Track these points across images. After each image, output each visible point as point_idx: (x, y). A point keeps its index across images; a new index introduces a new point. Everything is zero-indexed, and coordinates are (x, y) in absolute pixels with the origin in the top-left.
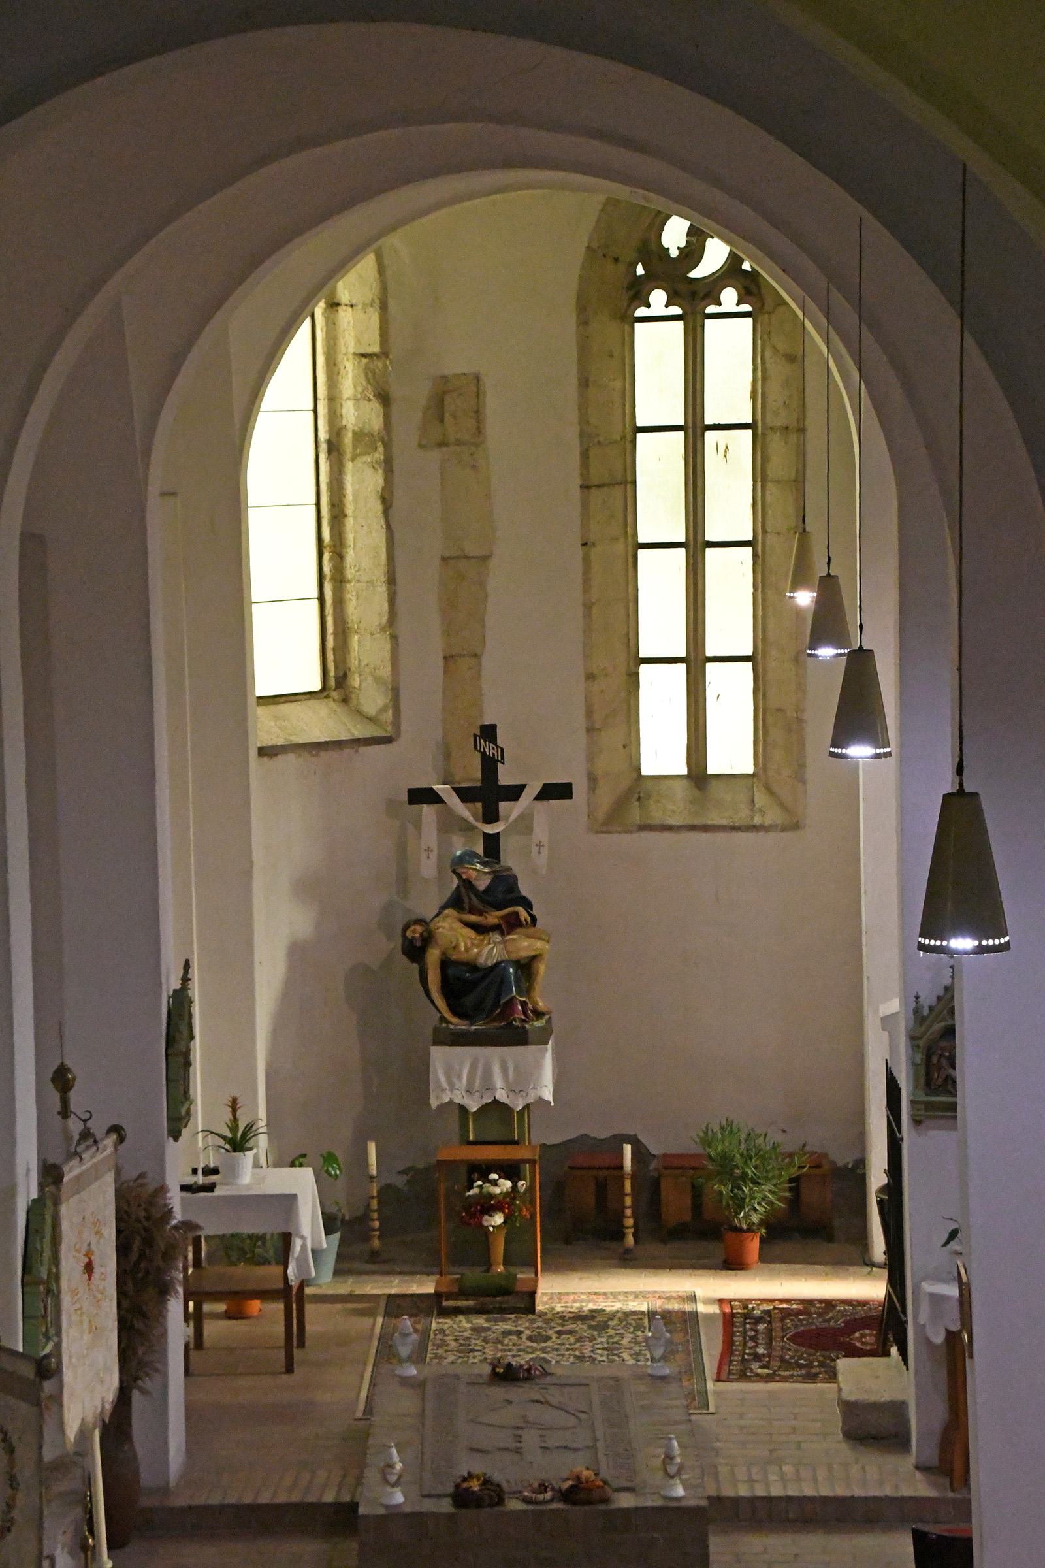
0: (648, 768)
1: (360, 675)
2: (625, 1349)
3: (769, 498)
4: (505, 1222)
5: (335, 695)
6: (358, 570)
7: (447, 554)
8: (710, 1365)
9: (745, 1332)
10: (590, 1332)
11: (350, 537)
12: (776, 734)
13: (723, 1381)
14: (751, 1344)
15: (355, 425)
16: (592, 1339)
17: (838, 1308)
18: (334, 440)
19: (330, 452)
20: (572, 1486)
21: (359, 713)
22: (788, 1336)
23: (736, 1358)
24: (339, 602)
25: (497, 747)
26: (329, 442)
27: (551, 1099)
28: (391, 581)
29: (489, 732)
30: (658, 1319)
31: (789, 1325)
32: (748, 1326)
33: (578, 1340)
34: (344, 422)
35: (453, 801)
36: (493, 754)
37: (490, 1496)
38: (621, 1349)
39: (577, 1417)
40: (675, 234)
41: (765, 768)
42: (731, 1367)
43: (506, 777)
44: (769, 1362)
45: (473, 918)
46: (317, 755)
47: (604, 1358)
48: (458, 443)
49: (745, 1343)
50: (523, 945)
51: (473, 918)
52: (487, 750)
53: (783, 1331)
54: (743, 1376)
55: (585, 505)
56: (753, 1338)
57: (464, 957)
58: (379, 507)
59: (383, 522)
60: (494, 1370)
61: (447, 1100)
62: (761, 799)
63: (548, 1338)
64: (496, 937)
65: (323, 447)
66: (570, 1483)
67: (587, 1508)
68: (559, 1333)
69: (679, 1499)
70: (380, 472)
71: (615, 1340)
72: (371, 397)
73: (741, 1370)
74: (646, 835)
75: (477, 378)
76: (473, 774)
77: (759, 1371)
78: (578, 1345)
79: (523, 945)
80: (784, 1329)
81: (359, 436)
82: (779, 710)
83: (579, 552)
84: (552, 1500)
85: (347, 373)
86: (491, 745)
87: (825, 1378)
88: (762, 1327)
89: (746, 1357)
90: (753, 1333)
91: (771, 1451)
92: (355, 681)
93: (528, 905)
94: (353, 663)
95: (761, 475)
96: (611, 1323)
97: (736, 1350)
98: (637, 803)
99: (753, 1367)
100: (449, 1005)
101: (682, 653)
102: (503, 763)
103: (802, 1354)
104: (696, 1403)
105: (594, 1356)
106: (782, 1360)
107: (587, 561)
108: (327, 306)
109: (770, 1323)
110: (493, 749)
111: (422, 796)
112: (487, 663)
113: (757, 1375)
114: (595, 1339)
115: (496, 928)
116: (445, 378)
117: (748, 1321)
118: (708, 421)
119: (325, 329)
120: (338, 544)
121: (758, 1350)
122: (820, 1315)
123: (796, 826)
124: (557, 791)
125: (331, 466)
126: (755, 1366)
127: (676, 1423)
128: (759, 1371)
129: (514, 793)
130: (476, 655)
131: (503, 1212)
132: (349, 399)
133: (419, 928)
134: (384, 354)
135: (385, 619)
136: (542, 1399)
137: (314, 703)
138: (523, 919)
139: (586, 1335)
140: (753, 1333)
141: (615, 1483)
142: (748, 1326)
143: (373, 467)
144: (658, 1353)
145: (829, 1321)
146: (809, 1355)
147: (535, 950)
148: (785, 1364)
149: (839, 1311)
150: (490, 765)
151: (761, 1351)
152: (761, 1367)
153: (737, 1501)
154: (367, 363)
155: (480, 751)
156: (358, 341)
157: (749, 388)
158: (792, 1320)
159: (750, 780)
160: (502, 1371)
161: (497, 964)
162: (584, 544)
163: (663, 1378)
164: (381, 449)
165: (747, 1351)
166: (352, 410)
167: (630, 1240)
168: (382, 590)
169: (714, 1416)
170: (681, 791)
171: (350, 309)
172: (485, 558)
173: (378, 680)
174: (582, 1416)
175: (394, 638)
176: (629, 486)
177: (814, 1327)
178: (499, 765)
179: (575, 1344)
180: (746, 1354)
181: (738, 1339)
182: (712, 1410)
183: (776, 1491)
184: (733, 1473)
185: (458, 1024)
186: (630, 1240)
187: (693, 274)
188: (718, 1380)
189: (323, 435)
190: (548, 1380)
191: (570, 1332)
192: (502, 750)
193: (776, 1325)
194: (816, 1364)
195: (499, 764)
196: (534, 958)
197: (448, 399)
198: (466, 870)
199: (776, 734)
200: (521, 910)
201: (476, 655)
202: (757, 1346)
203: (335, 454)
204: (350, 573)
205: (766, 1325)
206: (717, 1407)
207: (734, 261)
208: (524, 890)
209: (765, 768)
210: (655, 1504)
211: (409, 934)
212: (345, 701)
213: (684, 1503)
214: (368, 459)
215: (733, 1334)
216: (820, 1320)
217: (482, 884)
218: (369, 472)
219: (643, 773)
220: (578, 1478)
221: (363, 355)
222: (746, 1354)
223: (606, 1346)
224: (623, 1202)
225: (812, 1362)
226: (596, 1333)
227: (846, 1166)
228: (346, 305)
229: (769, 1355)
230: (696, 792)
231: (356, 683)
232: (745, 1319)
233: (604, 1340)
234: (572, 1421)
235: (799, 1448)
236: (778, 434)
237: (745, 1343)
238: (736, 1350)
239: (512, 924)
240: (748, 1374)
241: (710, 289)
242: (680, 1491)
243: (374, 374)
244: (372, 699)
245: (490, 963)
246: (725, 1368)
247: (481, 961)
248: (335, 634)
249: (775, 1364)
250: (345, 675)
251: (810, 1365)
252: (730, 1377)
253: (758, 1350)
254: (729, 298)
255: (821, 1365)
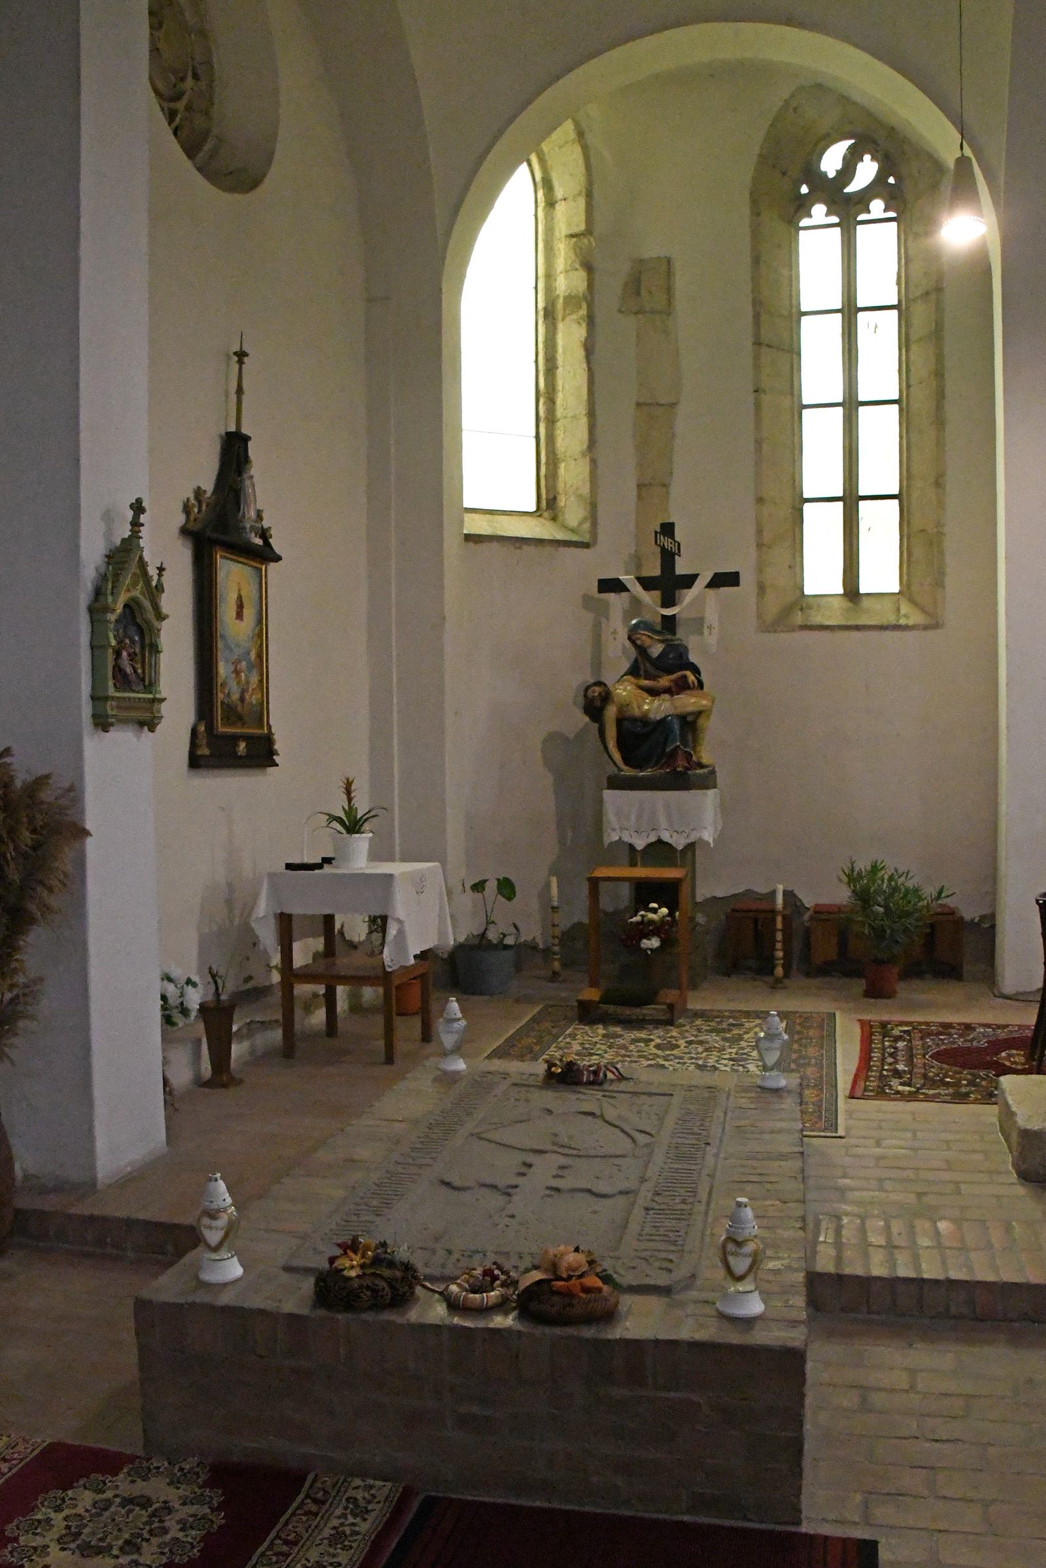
0: (811, 587)
1: (566, 495)
2: (753, 1060)
3: (912, 358)
4: (661, 946)
5: (546, 514)
6: (565, 409)
7: (642, 400)
8: (844, 1083)
9: (884, 1049)
10: (722, 1043)
11: (560, 383)
12: (918, 552)
13: (857, 1098)
14: (890, 1060)
15: (565, 292)
16: (722, 1049)
17: (978, 1030)
18: (550, 308)
19: (546, 316)
20: (540, 1282)
21: (564, 527)
22: (930, 1053)
23: (873, 1074)
24: (551, 438)
25: (675, 541)
26: (545, 309)
27: (711, 841)
28: (591, 414)
29: (668, 529)
30: (773, 1015)
31: (929, 1044)
32: (887, 1044)
33: (706, 1050)
34: (558, 292)
35: (637, 589)
36: (671, 548)
37: (375, 1291)
38: (749, 1059)
39: (634, 1141)
40: (831, 161)
41: (909, 587)
42: (868, 1083)
43: (682, 567)
44: (911, 1079)
45: (646, 683)
46: (520, 548)
47: (728, 1069)
48: (653, 312)
49: (883, 1060)
50: (688, 702)
51: (646, 683)
52: (666, 545)
53: (924, 1050)
54: (881, 1093)
55: (757, 358)
56: (891, 1055)
57: (636, 713)
58: (581, 353)
59: (585, 366)
60: (549, 1068)
61: (617, 838)
62: (905, 608)
63: (678, 1046)
64: (666, 696)
65: (541, 313)
66: (537, 1276)
67: (558, 1331)
68: (690, 1043)
69: (748, 1323)
70: (584, 325)
71: (745, 1051)
72: (578, 267)
73: (879, 1087)
74: (806, 634)
75: (669, 261)
76: (654, 569)
77: (900, 1088)
78: (704, 1054)
79: (688, 702)
80: (926, 1047)
81: (570, 300)
82: (922, 531)
83: (751, 398)
84: (501, 1306)
85: (560, 253)
86: (670, 540)
87: (978, 1099)
88: (901, 1044)
89: (885, 1073)
90: (892, 1050)
91: (920, 1195)
92: (562, 501)
93: (696, 671)
94: (560, 485)
95: (905, 342)
96: (746, 1036)
97: (875, 1048)
98: (800, 613)
99: (892, 1083)
100: (623, 758)
101: (841, 494)
102: (680, 556)
103: (947, 1072)
104: (822, 1124)
105: (717, 1066)
106: (925, 1076)
107: (758, 406)
108: (546, 205)
109: (910, 1041)
110: (671, 543)
111: (611, 586)
112: (675, 490)
113: (898, 1092)
114: (724, 1050)
115: (668, 691)
116: (641, 261)
117: (887, 1039)
118: (861, 493)
119: (544, 221)
120: (551, 390)
121: (897, 1066)
122: (961, 1036)
123: (934, 625)
124: (725, 580)
125: (546, 328)
126: (895, 1083)
127: (783, 1157)
128: (900, 1088)
129: (689, 581)
130: (664, 485)
131: (660, 937)
132: (561, 273)
133: (598, 689)
134: (589, 232)
135: (585, 446)
136: (598, 1112)
137: (529, 519)
138: (690, 682)
139: (717, 1045)
140: (892, 1050)
141: (627, 1278)
142: (886, 1043)
143: (579, 323)
144: (772, 1058)
145: (972, 1040)
146: (956, 1073)
147: (702, 706)
148: (933, 1084)
149: (980, 1033)
150: (668, 558)
151: (901, 1067)
152: (901, 1084)
153: (867, 1282)
154: (576, 243)
155: (660, 545)
156: (569, 225)
157: (895, 277)
158: (932, 1040)
159: (895, 598)
160: (560, 1070)
161: (664, 720)
162: (756, 391)
163: (777, 1091)
164: (584, 306)
165: (886, 1067)
166: (563, 280)
167: (779, 971)
168: (584, 421)
169: (843, 1140)
170: (837, 604)
171: (563, 202)
172: (673, 405)
173: (580, 497)
174: (641, 1139)
175: (593, 462)
176: (795, 356)
177: (956, 1046)
178: (677, 557)
179: (701, 1053)
180: (885, 1070)
181: (876, 1055)
182: (841, 1132)
183: (930, 1271)
184: (863, 1230)
185: (628, 771)
186: (779, 971)
187: (848, 190)
188: (852, 1097)
189: (541, 305)
190: (622, 1086)
191: (701, 1043)
192: (679, 544)
193: (917, 1043)
194: (965, 1082)
195: (659, 531)
196: (699, 714)
197: (644, 277)
198: (639, 636)
199: (918, 552)
200: (688, 673)
201: (664, 485)
202: (896, 1062)
203: (550, 318)
204: (559, 412)
205: (905, 1043)
206: (848, 1129)
207: (880, 179)
208: (693, 658)
209: (909, 587)
210: (701, 1336)
211: (590, 694)
212: (554, 519)
213: (760, 1337)
214: (574, 317)
215: (871, 1050)
216: (961, 1040)
217: (656, 650)
218: (575, 326)
219: (806, 593)
220: (554, 1267)
221: (572, 236)
222: (885, 1070)
223: (733, 1056)
224: (774, 936)
225: (959, 1081)
226: (727, 1044)
227: (972, 920)
228: (561, 200)
229: (910, 1072)
230: (850, 604)
231: (562, 504)
232: (884, 1037)
233: (734, 1051)
234: (625, 1145)
235: (958, 1192)
236: (919, 301)
237: (883, 1060)
238: (874, 1066)
239: (682, 686)
240: (887, 1091)
241: (862, 200)
242: (755, 1306)
243: (581, 249)
244: (574, 513)
245: (658, 718)
246: (862, 1084)
247: (652, 716)
248: (547, 463)
249: (919, 1082)
250: (555, 498)
251: (957, 1084)
252: (866, 1094)
253: (897, 1066)
254: (877, 207)
255: (971, 1083)
